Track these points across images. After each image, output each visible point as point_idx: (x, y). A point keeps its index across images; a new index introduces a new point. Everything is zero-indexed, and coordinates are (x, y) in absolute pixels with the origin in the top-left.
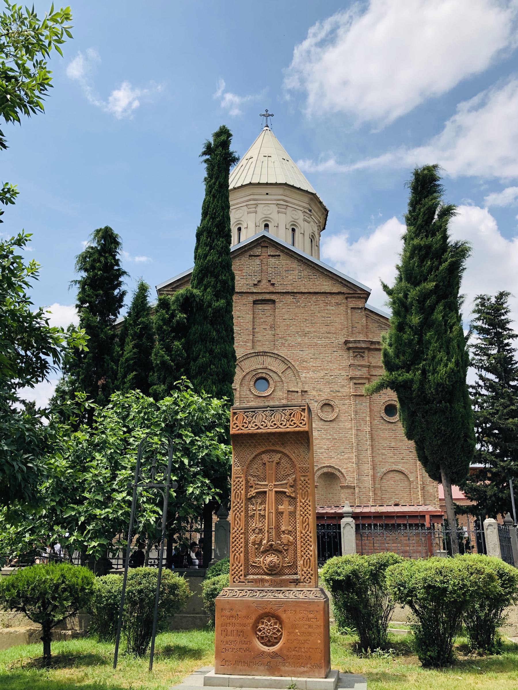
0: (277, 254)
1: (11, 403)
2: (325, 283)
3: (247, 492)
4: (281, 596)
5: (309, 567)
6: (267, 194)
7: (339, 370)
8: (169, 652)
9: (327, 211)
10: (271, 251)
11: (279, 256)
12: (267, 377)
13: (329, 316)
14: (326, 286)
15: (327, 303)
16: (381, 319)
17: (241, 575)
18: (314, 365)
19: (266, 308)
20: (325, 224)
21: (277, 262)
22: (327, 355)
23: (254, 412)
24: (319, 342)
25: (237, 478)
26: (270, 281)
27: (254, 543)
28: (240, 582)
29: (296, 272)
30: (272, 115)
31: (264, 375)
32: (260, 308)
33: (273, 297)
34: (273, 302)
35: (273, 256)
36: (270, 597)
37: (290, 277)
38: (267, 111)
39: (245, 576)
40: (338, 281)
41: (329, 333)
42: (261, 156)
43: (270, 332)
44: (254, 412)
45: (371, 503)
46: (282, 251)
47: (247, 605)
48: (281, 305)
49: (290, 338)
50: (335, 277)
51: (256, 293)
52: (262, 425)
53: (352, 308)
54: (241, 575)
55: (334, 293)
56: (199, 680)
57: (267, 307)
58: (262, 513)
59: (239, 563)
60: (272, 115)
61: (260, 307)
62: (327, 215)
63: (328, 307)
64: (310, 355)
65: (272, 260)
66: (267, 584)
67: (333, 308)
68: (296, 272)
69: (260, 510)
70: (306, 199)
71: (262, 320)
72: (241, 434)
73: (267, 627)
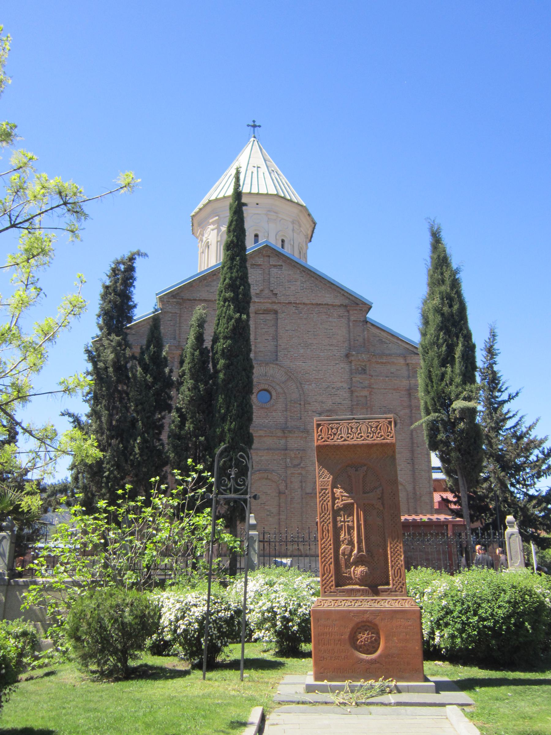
0: (279, 264)
1: (184, 410)
2: (327, 296)
3: (333, 504)
4: (376, 605)
5: (400, 577)
6: (257, 204)
7: (341, 382)
8: (234, 665)
9: (315, 224)
10: (273, 261)
11: (282, 266)
12: (270, 388)
13: (332, 328)
14: (328, 298)
15: (329, 315)
16: (382, 333)
17: (332, 586)
18: (317, 377)
19: (268, 318)
20: (312, 237)
21: (279, 272)
22: (329, 367)
23: (339, 424)
24: (321, 354)
25: (322, 490)
26: (272, 291)
27: (344, 554)
28: (331, 592)
29: (298, 283)
30: (260, 126)
31: (266, 387)
32: (262, 318)
33: (275, 307)
34: (276, 312)
35: (275, 266)
36: (365, 606)
37: (293, 288)
38: (254, 121)
39: (336, 586)
40: (340, 293)
41: (331, 345)
42: (250, 166)
43: (272, 343)
44: (339, 424)
45: (350, 518)
46: (284, 262)
47: (344, 615)
48: (283, 315)
49: (292, 350)
50: (337, 289)
51: (258, 302)
52: (348, 437)
53: (354, 321)
54: (332, 586)
55: (336, 306)
56: (301, 689)
57: (270, 317)
58: (350, 524)
59: (330, 573)
60: (260, 126)
61: (261, 316)
62: (314, 228)
63: (330, 319)
64: (312, 367)
65: (274, 271)
66: (359, 594)
67: (335, 320)
68: (298, 283)
69: (348, 522)
70: (295, 210)
71: (264, 330)
72: (327, 445)
73: (364, 637)
